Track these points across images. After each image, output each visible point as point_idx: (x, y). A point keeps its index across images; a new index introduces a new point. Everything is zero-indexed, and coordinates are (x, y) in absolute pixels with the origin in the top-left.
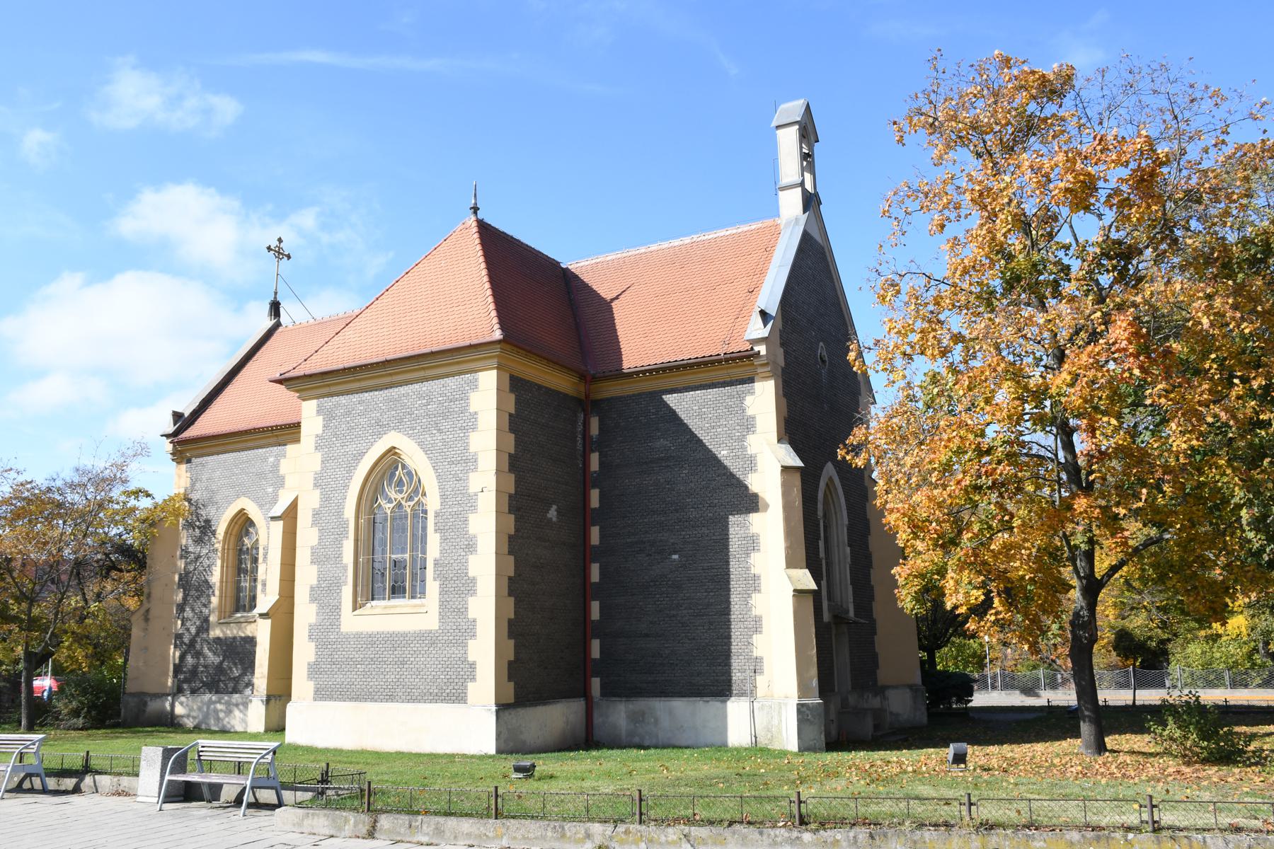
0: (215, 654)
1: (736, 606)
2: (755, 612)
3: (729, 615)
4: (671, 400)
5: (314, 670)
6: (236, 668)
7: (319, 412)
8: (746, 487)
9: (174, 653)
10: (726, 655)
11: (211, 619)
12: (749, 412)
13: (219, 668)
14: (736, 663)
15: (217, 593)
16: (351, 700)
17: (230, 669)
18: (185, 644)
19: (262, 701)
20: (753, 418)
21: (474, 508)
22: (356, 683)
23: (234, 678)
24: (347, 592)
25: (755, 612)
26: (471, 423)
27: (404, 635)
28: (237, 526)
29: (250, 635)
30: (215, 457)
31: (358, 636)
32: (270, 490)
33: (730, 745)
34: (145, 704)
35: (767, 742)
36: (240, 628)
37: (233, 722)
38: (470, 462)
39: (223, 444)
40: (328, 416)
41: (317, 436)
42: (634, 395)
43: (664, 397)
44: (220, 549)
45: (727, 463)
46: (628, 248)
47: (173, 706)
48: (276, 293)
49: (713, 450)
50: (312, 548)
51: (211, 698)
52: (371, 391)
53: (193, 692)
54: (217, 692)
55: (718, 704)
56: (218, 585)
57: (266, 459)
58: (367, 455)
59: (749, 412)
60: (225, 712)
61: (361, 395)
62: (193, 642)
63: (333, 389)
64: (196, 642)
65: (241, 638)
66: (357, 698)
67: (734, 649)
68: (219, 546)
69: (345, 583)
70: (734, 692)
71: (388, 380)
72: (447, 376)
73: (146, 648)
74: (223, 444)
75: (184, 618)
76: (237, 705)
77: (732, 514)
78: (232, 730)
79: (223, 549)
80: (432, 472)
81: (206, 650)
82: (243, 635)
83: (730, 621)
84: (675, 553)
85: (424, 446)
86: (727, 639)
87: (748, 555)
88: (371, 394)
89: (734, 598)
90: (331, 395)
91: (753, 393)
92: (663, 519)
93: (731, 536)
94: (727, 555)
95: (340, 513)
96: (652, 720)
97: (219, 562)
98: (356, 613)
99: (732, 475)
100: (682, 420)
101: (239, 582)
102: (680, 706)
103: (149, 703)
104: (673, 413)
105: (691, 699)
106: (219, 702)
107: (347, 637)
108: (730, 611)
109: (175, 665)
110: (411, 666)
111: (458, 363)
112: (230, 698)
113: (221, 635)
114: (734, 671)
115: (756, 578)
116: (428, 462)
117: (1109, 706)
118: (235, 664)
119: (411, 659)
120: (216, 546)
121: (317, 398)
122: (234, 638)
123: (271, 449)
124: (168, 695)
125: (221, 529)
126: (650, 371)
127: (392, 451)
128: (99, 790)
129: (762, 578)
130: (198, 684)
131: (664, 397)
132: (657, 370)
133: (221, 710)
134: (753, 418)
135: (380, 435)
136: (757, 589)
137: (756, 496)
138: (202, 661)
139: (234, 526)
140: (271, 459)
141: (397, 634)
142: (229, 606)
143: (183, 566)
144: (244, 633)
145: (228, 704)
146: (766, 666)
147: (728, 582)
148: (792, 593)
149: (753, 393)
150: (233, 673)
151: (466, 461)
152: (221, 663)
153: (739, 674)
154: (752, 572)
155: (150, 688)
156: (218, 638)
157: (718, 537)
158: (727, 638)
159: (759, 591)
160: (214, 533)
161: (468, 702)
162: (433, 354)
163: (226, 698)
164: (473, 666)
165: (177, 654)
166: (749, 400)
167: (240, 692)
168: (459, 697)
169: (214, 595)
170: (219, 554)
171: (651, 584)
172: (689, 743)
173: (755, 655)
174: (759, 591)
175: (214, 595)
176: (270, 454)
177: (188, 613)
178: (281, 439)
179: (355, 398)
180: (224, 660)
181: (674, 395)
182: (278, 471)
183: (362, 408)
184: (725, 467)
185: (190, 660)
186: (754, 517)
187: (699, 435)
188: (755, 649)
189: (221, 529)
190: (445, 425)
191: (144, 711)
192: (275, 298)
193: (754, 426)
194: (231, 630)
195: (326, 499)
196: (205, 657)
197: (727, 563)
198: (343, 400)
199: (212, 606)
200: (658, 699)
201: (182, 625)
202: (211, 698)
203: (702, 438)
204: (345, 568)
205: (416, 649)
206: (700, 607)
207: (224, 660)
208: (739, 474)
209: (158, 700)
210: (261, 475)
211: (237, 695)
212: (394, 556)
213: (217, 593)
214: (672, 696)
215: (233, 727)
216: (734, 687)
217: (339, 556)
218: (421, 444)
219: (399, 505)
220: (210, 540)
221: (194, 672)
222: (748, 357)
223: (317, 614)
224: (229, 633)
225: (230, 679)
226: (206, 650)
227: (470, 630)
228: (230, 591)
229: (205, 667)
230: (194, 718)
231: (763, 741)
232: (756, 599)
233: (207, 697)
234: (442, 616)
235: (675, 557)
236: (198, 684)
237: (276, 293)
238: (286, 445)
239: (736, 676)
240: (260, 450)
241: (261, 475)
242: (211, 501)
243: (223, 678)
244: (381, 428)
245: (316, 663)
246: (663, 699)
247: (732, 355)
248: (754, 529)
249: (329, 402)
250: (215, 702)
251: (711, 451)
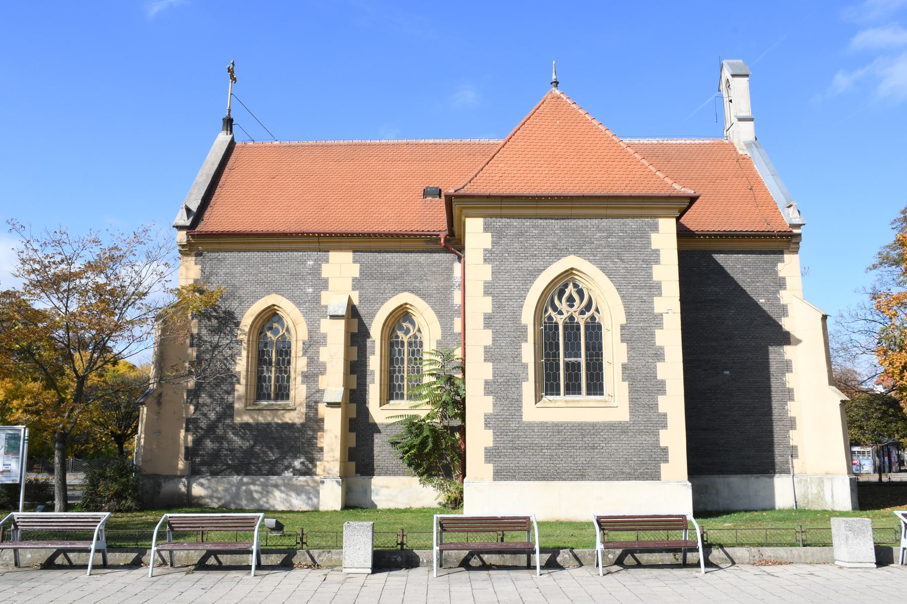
0: (242, 438)
1: (776, 410)
2: (790, 414)
3: (772, 416)
4: (720, 258)
5: (491, 455)
6: (272, 451)
7: (486, 229)
8: (781, 326)
9: (186, 438)
10: (771, 444)
11: (236, 406)
12: (781, 274)
13: (250, 452)
14: (777, 451)
15: (243, 381)
16: (537, 479)
17: (265, 453)
18: (201, 428)
19: (337, 481)
20: (784, 278)
21: (660, 325)
22: (541, 465)
23: (269, 461)
24: (528, 388)
25: (790, 414)
26: (654, 259)
27: (594, 425)
28: (262, 320)
29: (290, 422)
30: (236, 254)
31: (543, 425)
32: (310, 290)
33: (777, 508)
34: (160, 485)
35: (804, 505)
36: (276, 416)
37: (272, 502)
38: (656, 289)
39: (249, 243)
40: (498, 236)
41: (485, 250)
42: (687, 251)
43: (713, 255)
44: (246, 340)
45: (766, 308)
46: (622, 137)
47: (189, 488)
48: (230, 111)
49: (754, 298)
50: (486, 347)
51: (241, 480)
52: (546, 219)
53: (214, 474)
54: (246, 474)
55: (767, 479)
56: (243, 374)
57: (303, 262)
58: (544, 273)
59: (781, 274)
60: (261, 493)
61: (534, 221)
62: (212, 427)
63: (504, 212)
64: (217, 427)
65: (277, 424)
66: (544, 478)
67: (776, 440)
68: (244, 338)
69: (526, 379)
70: (777, 470)
71: (568, 212)
72: (627, 217)
73: (159, 432)
74: (249, 243)
75: (198, 403)
76: (276, 486)
77: (770, 345)
78: (272, 509)
79: (249, 341)
80: (617, 293)
81: (231, 435)
82: (280, 421)
83: (772, 421)
84: (727, 369)
85: (607, 271)
86: (771, 432)
87: (784, 374)
88: (547, 221)
89: (775, 404)
90: (501, 217)
91: (783, 262)
92: (715, 344)
93: (771, 360)
94: (768, 372)
95: (516, 316)
96: (714, 491)
97: (244, 353)
98: (382, 408)
99: (770, 318)
100: (729, 274)
101: (262, 372)
102: (737, 481)
103: (163, 484)
104: (722, 268)
105: (744, 476)
106: (254, 484)
107: (531, 426)
108: (771, 413)
109: (187, 448)
110: (602, 451)
111: (642, 208)
112: (267, 480)
113: (251, 421)
114: (776, 456)
115: (790, 391)
116: (611, 284)
117: (893, 482)
118: (271, 449)
119: (602, 445)
120: (240, 337)
121: (484, 217)
122: (269, 424)
123: (309, 253)
124: (182, 477)
125: (247, 321)
126: (716, 236)
127: (569, 272)
128: (736, 561)
129: (795, 391)
130: (220, 467)
131: (713, 255)
132: (721, 236)
133: (257, 491)
134: (784, 278)
135: (558, 257)
136: (791, 399)
137: (788, 333)
138: (225, 445)
139: (259, 320)
140: (311, 263)
141: (586, 424)
142: (253, 395)
143: (195, 354)
144: (281, 419)
145: (264, 486)
146: (800, 452)
147: (770, 392)
148: (840, 403)
149: (783, 262)
150: (268, 456)
151: (651, 287)
152: (252, 447)
153: (780, 458)
154: (787, 386)
155: (163, 470)
156: (247, 424)
157: (761, 361)
158: (770, 433)
159: (793, 400)
160: (237, 324)
161: (662, 478)
162: (546, 197)
163: (262, 480)
164: (665, 450)
165: (190, 438)
166: (780, 266)
167: (278, 474)
168: (655, 476)
169: (239, 383)
170: (245, 345)
171: (708, 391)
172: (746, 507)
173: (791, 444)
174: (793, 400)
175: (239, 383)
176: (310, 259)
177: (204, 398)
178: (322, 246)
179: (528, 223)
180: (255, 444)
181: (721, 255)
182: (320, 274)
183: (537, 232)
184: (764, 311)
185: (209, 444)
186: (787, 349)
187: (743, 287)
188: (791, 440)
189: (247, 321)
190: (627, 256)
191: (159, 492)
192: (229, 115)
193: (784, 284)
194: (264, 417)
195: (498, 306)
196: (230, 442)
197: (768, 379)
198: (515, 222)
199: (236, 394)
200: (717, 476)
201: (196, 410)
202: (241, 480)
203: (745, 289)
204: (525, 366)
205: (606, 437)
206: (748, 410)
207: (255, 444)
208: (774, 317)
209: (171, 481)
210: (296, 276)
211: (275, 477)
212: (567, 359)
213: (243, 381)
214: (727, 474)
215: (273, 506)
216: (777, 467)
217: (517, 356)
218: (603, 269)
219: (571, 318)
220: (231, 331)
221: (215, 456)
222: (787, 236)
223: (494, 405)
224: (261, 419)
225: (265, 462)
226: (231, 435)
227: (662, 421)
228: (254, 380)
229: (231, 450)
230: (219, 499)
231: (801, 504)
232: (790, 405)
233: (235, 479)
234: (632, 411)
235: (727, 372)
236: (220, 467)
237: (230, 111)
238: (329, 252)
239: (778, 459)
240: (296, 253)
241: (296, 276)
242: (232, 295)
243: (253, 461)
244: (558, 253)
245: (496, 448)
246: (721, 476)
247: (747, 233)
248: (787, 356)
249: (499, 223)
250: (247, 484)
251: (753, 299)
